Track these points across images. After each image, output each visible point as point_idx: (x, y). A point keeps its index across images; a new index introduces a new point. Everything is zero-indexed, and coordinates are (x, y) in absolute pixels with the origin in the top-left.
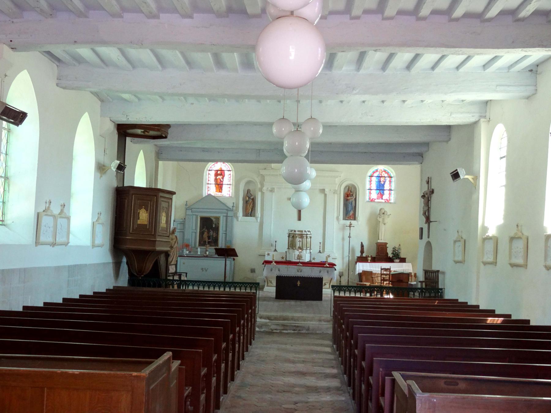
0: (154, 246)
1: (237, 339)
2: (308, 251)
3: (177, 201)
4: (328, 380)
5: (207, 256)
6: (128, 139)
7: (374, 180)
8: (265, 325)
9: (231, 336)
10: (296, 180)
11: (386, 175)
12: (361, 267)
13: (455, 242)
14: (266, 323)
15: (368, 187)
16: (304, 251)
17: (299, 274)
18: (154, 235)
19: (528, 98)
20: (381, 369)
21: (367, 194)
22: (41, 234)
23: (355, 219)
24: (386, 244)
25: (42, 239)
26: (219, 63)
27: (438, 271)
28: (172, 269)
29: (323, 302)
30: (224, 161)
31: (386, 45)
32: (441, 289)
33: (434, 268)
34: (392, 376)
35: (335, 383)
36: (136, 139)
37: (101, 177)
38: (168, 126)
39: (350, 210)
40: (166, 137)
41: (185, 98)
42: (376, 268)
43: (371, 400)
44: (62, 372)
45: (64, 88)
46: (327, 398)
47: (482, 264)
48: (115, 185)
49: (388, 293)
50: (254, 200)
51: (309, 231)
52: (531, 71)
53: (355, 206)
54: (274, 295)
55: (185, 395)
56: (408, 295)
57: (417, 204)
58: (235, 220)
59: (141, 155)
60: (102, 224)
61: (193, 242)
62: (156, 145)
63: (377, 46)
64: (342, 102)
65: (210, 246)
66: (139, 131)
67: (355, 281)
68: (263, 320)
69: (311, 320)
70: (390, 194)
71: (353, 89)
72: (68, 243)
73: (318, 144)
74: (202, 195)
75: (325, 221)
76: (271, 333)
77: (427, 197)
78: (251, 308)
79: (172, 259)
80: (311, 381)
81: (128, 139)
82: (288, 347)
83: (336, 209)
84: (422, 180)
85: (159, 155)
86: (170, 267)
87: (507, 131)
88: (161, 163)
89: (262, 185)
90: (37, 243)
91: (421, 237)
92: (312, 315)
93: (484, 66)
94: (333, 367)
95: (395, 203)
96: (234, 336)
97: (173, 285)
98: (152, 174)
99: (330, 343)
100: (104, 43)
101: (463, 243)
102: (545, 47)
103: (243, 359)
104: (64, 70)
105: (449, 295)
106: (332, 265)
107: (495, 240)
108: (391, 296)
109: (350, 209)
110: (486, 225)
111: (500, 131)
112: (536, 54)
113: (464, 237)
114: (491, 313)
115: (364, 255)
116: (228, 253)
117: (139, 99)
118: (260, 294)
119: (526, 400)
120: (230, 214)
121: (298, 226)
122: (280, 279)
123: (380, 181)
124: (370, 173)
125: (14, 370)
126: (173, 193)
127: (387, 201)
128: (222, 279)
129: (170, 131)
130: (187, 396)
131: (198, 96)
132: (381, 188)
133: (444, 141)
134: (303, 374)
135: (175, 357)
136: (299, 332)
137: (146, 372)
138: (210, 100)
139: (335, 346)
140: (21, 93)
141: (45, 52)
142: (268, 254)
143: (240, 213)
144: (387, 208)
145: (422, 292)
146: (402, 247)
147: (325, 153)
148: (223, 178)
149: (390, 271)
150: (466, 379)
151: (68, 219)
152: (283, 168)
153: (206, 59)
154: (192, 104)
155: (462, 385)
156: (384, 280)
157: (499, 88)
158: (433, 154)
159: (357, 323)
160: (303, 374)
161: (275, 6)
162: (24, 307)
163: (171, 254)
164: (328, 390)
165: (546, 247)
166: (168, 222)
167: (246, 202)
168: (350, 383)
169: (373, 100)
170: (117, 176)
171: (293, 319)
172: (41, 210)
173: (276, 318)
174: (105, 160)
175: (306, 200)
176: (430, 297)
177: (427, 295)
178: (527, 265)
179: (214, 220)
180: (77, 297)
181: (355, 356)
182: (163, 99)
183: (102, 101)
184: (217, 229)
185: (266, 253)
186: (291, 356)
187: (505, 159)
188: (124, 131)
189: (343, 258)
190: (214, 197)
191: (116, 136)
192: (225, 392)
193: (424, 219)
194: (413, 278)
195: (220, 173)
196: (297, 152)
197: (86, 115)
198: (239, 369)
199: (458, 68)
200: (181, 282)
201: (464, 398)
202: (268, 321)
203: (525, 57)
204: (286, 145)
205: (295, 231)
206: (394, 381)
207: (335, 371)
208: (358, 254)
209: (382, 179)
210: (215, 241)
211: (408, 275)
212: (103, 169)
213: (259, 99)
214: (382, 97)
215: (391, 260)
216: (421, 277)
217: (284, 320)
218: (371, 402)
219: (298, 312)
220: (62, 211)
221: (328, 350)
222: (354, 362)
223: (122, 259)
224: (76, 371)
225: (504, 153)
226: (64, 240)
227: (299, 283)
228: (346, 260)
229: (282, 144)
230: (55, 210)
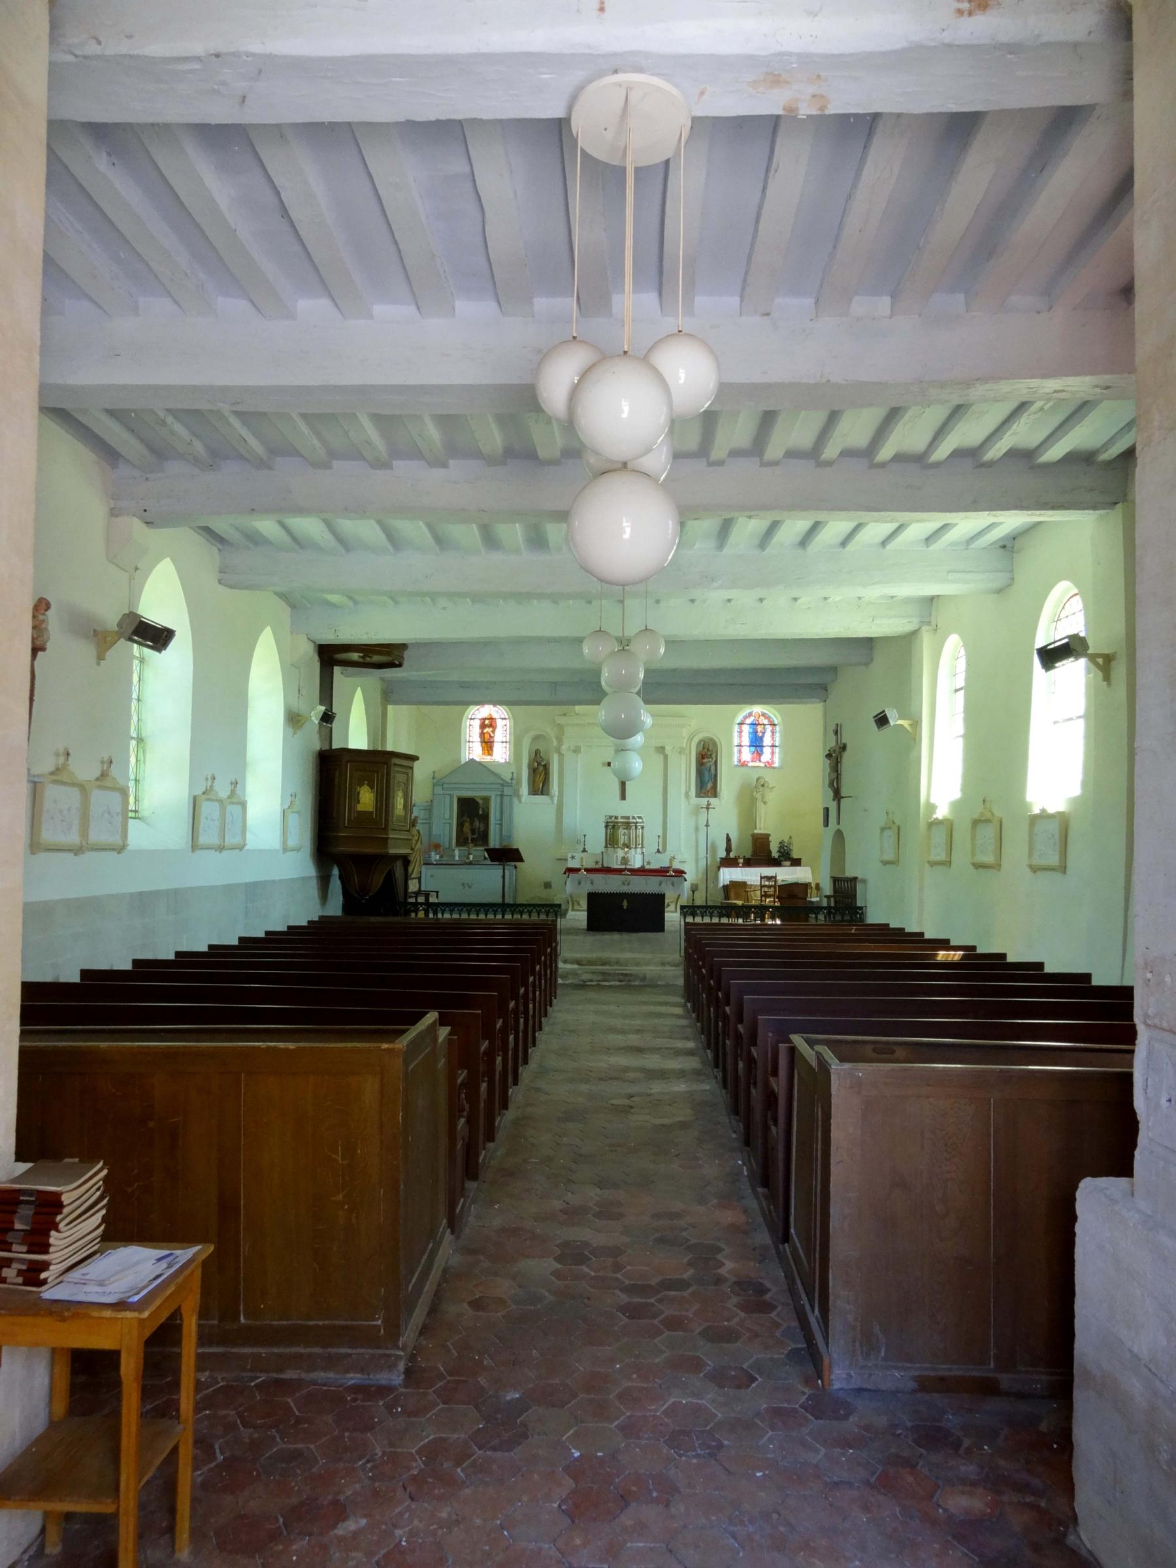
0: (386, 847)
1: (531, 995)
2: (639, 850)
3: (421, 772)
4: (680, 1059)
5: (470, 863)
7: (746, 729)
8: (574, 974)
9: (522, 990)
10: (622, 731)
11: (766, 722)
12: (728, 875)
13: (883, 829)
14: (574, 970)
15: (736, 741)
18: (385, 829)
19: (999, 591)
20: (770, 1035)
21: (737, 752)
22: (201, 831)
23: (715, 795)
24: (768, 835)
25: (203, 839)
26: (490, 541)
27: (855, 879)
28: (413, 886)
29: (666, 934)
30: (495, 703)
31: (765, 507)
32: (861, 908)
33: (849, 873)
34: (790, 1041)
35: (693, 1063)
36: (350, 669)
37: (295, 733)
38: (404, 646)
39: (706, 777)
40: (400, 665)
41: (433, 600)
42: (752, 876)
43: (755, 1084)
44: (269, 1048)
45: (231, 587)
46: (681, 1087)
47: (927, 865)
48: (317, 746)
49: (773, 918)
50: (546, 768)
51: (640, 818)
52: (1004, 547)
53: (716, 775)
54: (584, 924)
55: (459, 1081)
56: (807, 919)
57: (818, 768)
58: (515, 800)
59: (359, 696)
60: (298, 812)
61: (447, 839)
62: (382, 679)
63: (752, 508)
64: (693, 601)
65: (476, 845)
66: (355, 656)
67: (719, 899)
68: (569, 966)
69: (648, 964)
70: (773, 753)
71: (713, 580)
72: (245, 845)
73: (654, 671)
74: (459, 760)
75: (669, 800)
76: (582, 986)
77: (835, 757)
78: (550, 946)
79: (414, 870)
80: (653, 1062)
82: (612, 1008)
83: (683, 776)
84: (825, 729)
85: (389, 695)
86: (410, 882)
87: (965, 645)
88: (390, 707)
89: (560, 741)
90: (195, 846)
91: (826, 824)
92: (649, 956)
93: (927, 539)
94: (687, 1039)
95: (780, 768)
96: (526, 991)
97: (416, 912)
98: (378, 726)
100: (300, 511)
101: (895, 830)
102: (1027, 508)
103: (541, 1029)
104: (230, 555)
105: (874, 917)
106: (680, 873)
107: (948, 826)
108: (778, 922)
109: (706, 779)
110: (932, 801)
111: (953, 644)
112: (1011, 521)
113: (897, 822)
114: (944, 944)
115: (732, 855)
116: (507, 856)
117: (356, 602)
118: (561, 923)
119: (1001, 1071)
120: (507, 791)
121: (622, 810)
122: (593, 898)
123: (756, 732)
124: (739, 719)
125: (190, 1047)
126: (414, 758)
127: (769, 765)
128: (500, 900)
129: (406, 654)
130: (462, 1084)
131: (452, 596)
132: (757, 743)
133: (860, 664)
134: (639, 1050)
135: (443, 1021)
136: (629, 983)
137: (402, 1043)
138: (473, 602)
139: (689, 1005)
140: (162, 598)
141: (199, 527)
142: (573, 857)
143: (524, 789)
144: (769, 777)
145: (829, 913)
146: (795, 841)
147: (669, 686)
148: (493, 732)
149: (776, 881)
150: (906, 1043)
151: (243, 805)
152: (601, 713)
153: (467, 533)
154: (444, 608)
155: (900, 1052)
156: (766, 895)
157: (951, 576)
158: (844, 687)
159: (728, 964)
160: (639, 1050)
161: (597, 453)
162: (178, 954)
163: (411, 859)
164: (681, 1074)
165: (1031, 835)
166: (408, 806)
167: (533, 771)
168: (718, 1061)
169: (744, 598)
170: (320, 732)
171: (617, 962)
172: (199, 792)
173: (591, 963)
174: (300, 706)
175: (636, 765)
176: (843, 921)
177: (838, 918)
178: (1000, 865)
179: (481, 802)
180: (205, 949)
181: (725, 1017)
182: (397, 603)
183: (293, 607)
184: (485, 818)
185: (570, 855)
186: (618, 1023)
187: (962, 692)
188: (331, 656)
189: (697, 861)
190: (480, 763)
191: (317, 665)
192: (516, 1083)
193: (831, 794)
194: (814, 891)
195: (488, 724)
196: (622, 686)
197: (268, 631)
198: (534, 1045)
199: (884, 543)
200: (428, 906)
201: (906, 1069)
202: (576, 966)
203: (992, 526)
204: (605, 674)
205: (616, 818)
206: (793, 1050)
207: (691, 1045)
208: (722, 853)
209: (759, 728)
210: (483, 837)
211: (806, 886)
212: (299, 721)
213: (555, 598)
214: (760, 592)
215: (776, 863)
216: (828, 889)
217: (604, 964)
218: (755, 1087)
219: (628, 951)
220: (233, 792)
221: (679, 1011)
222: (724, 1026)
223: (331, 870)
224: (291, 1046)
225: (960, 682)
226: (237, 840)
227: (625, 904)
228: (702, 864)
229: (597, 673)
230: (223, 791)
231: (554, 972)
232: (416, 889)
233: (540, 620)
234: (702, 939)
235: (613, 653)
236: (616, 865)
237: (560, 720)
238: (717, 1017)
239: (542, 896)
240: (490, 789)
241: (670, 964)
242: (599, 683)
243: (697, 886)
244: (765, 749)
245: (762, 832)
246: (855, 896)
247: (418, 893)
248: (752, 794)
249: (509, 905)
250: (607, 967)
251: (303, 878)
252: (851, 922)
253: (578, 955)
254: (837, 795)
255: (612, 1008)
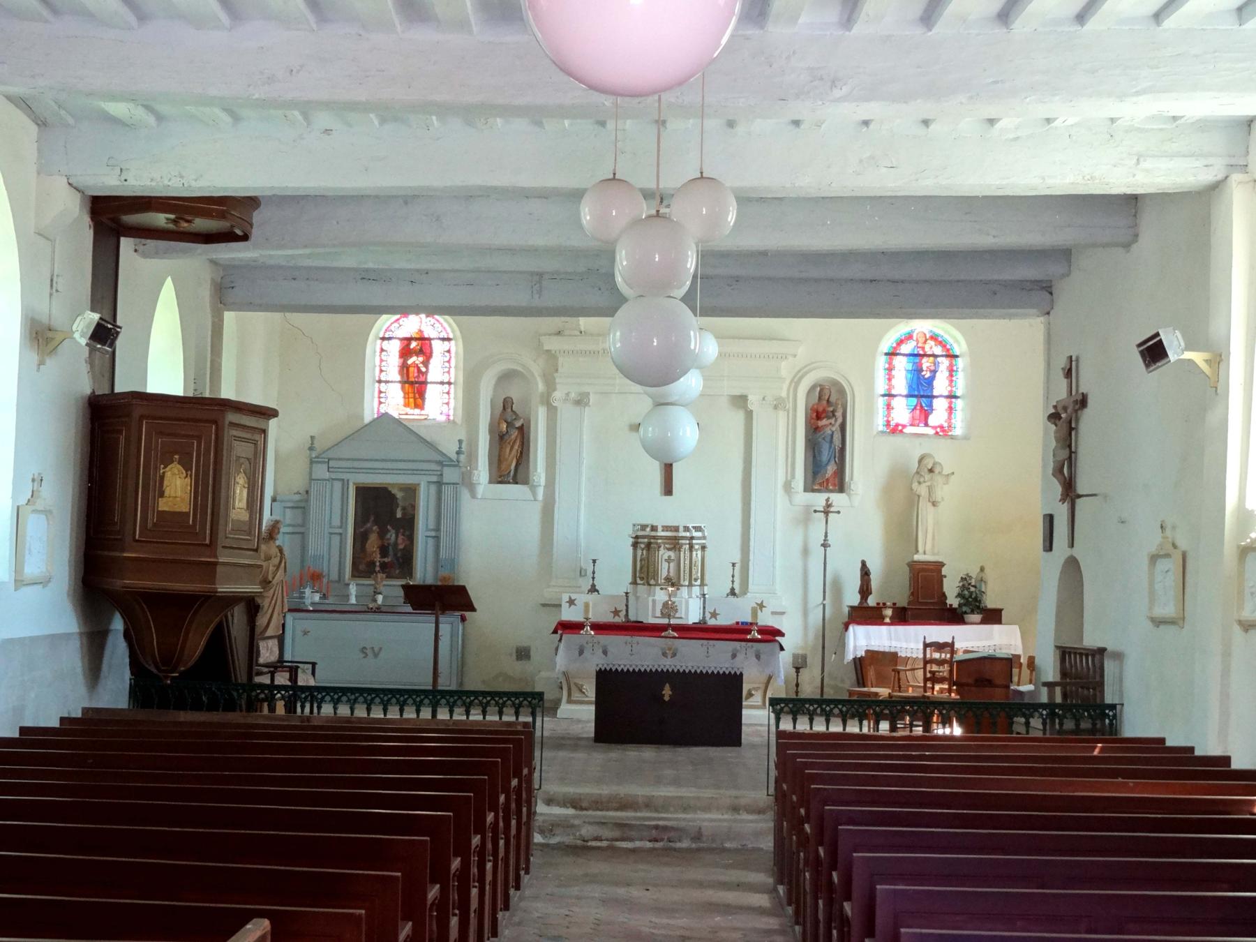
2: (696, 590)
3: (281, 438)
5: (378, 610)
6: (126, 244)
7: (902, 364)
9: (456, 863)
10: (655, 373)
11: (938, 350)
12: (862, 639)
13: (1154, 559)
16: (684, 591)
17: (668, 664)
18: (212, 546)
23: (841, 488)
24: (942, 565)
27: (1102, 651)
28: (268, 652)
30: (431, 311)
32: (1113, 707)
33: (1091, 639)
36: (151, 243)
38: (252, 202)
40: (245, 238)
41: (306, 116)
42: (908, 641)
48: (86, 386)
51: (698, 529)
54: (590, 729)
57: (1033, 442)
58: (465, 494)
59: (168, 292)
60: (47, 512)
62: (214, 262)
64: (797, 123)
66: (161, 219)
67: (843, 685)
68: (557, 811)
69: (707, 808)
70: (951, 409)
71: (834, 83)
74: (363, 419)
76: (580, 850)
77: (1066, 419)
78: (518, 774)
79: (269, 620)
81: (126, 244)
82: (636, 892)
85: (225, 293)
88: (229, 317)
89: (551, 385)
91: (1049, 546)
92: (708, 793)
95: (966, 438)
96: (465, 865)
98: (204, 351)
99: (765, 879)
105: (1136, 725)
106: (771, 634)
108: (957, 731)
109: (825, 458)
110: (1250, 505)
113: (1183, 544)
115: (871, 601)
116: (446, 598)
117: (160, 118)
118: (546, 726)
120: (450, 475)
121: (664, 513)
122: (607, 681)
123: (918, 370)
126: (273, 413)
127: (943, 431)
129: (257, 217)
131: (344, 108)
136: (669, 845)
138: (383, 121)
142: (571, 602)
143: (482, 472)
144: (942, 453)
145: (1052, 715)
146: (990, 575)
147: (743, 284)
148: (426, 363)
149: (953, 652)
152: (614, 335)
156: (934, 679)
163: (265, 603)
167: (499, 439)
169: (894, 118)
171: (649, 804)
173: (598, 804)
174: (54, 311)
175: (686, 433)
176: (1077, 731)
177: (1069, 725)
179: (399, 495)
181: (844, 921)
182: (236, 118)
183: (42, 124)
184: (408, 524)
185: (565, 598)
189: (805, 613)
190: (398, 422)
191: (88, 235)
193: (1058, 489)
196: (657, 286)
200: (296, 693)
202: (571, 811)
204: (623, 261)
205: (654, 528)
209: (926, 363)
210: (405, 562)
211: (1010, 663)
212: (48, 341)
213: (537, 115)
215: (954, 617)
216: (1050, 670)
219: (669, 782)
221: (763, 900)
223: (109, 620)
227: (667, 692)
228: (816, 617)
229: (608, 254)
231: (526, 827)
232: (274, 657)
233: (508, 156)
234: (807, 766)
235: (637, 222)
236: (652, 617)
237: (552, 344)
238: (829, 921)
239: (511, 674)
240: (415, 472)
241: (750, 810)
242: (612, 276)
243: (804, 657)
244: (936, 402)
245: (929, 558)
246: (1101, 684)
247: (278, 665)
248: (907, 494)
249: (444, 693)
250: (630, 814)
251: (53, 637)
252: (1095, 734)
253: (571, 790)
254: (1070, 491)
255: (636, 892)
